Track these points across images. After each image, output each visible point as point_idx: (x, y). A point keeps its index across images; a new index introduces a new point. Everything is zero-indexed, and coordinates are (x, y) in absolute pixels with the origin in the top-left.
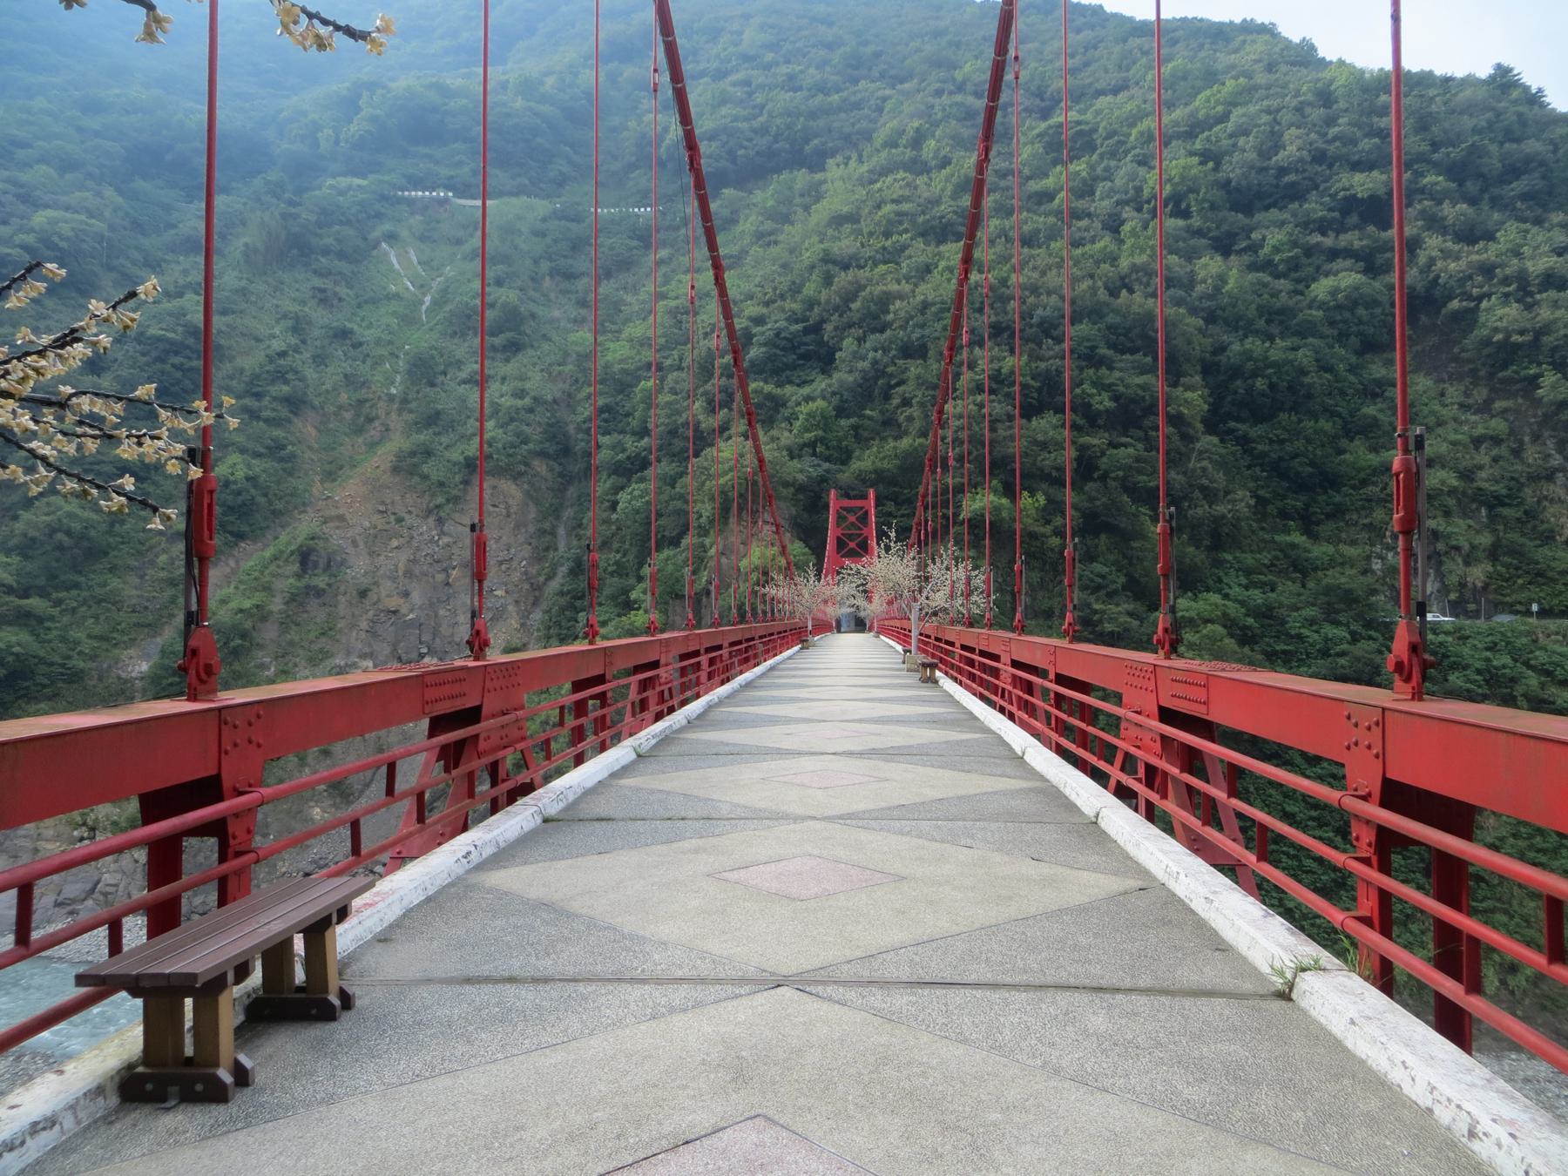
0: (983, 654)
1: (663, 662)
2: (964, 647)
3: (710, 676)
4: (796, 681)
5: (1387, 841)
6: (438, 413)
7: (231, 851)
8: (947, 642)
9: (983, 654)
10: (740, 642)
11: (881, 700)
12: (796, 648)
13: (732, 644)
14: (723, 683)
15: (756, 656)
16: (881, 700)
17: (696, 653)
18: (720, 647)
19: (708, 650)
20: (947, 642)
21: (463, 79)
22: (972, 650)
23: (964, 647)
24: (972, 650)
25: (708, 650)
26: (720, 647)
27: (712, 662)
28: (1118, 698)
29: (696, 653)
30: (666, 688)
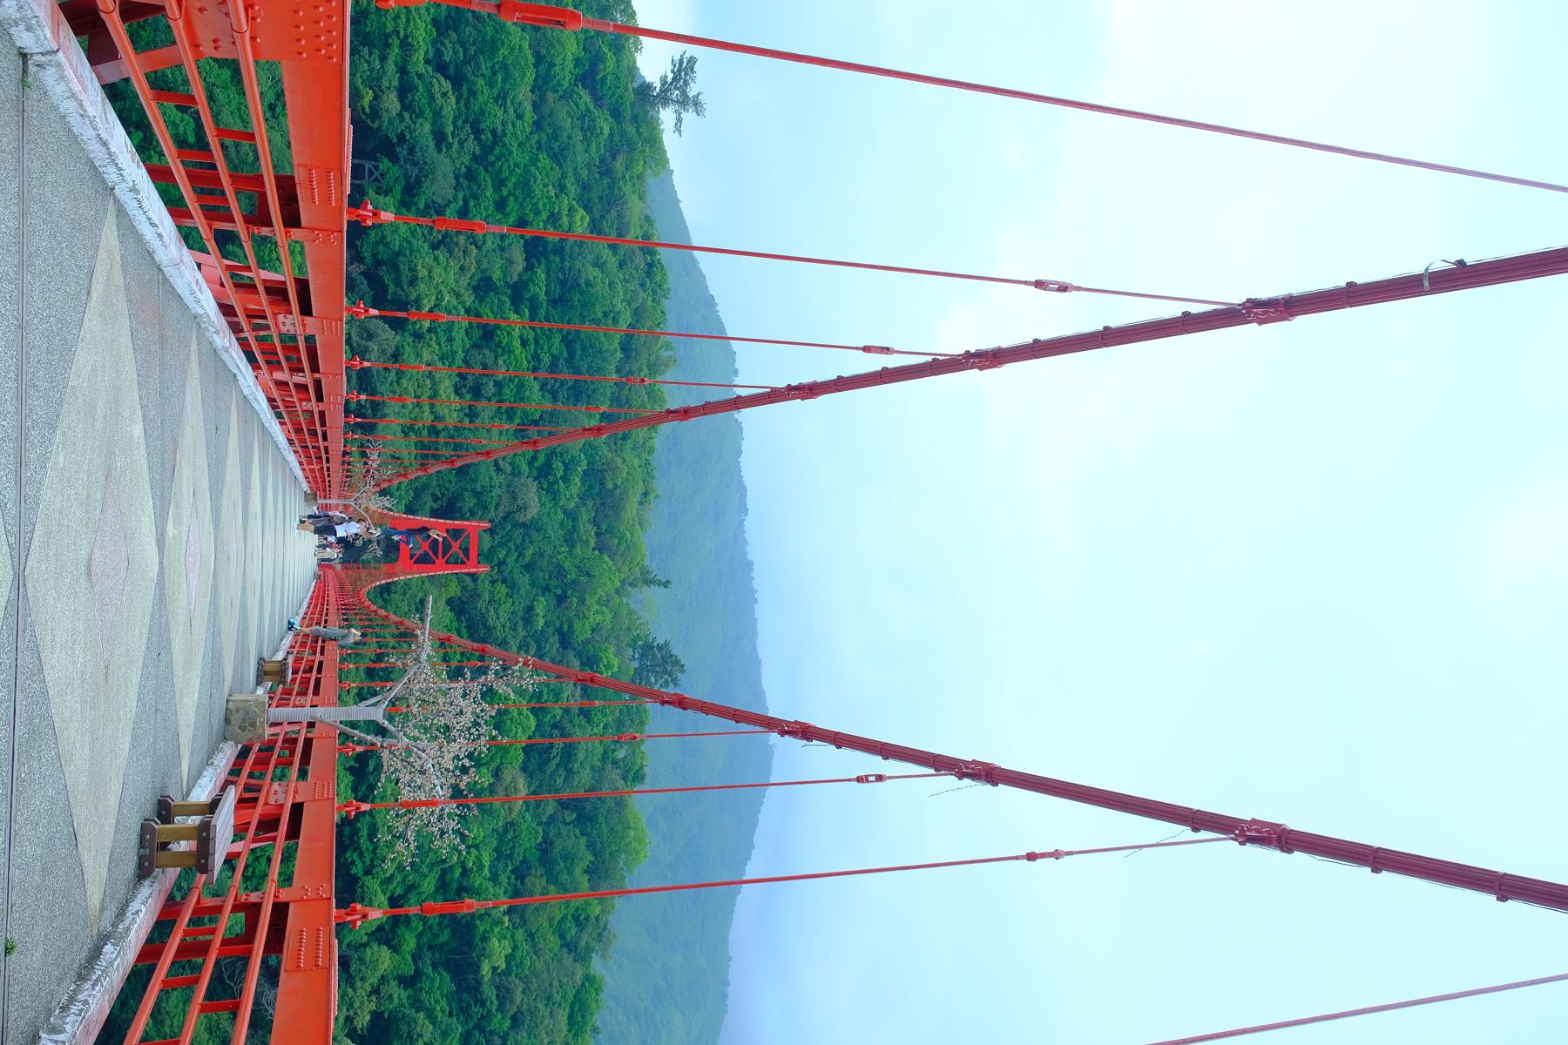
0: (318, 681)
1: (308, 319)
2: (321, 663)
3: (281, 385)
4: (270, 493)
5: (252, 910)
6: (578, 400)
7: (228, 141)
8: (323, 648)
9: (318, 681)
10: (323, 424)
11: (261, 615)
12: (305, 486)
13: (322, 414)
14: (271, 400)
15: (225, 241)
16: (261, 615)
17: (315, 368)
18: (320, 398)
19: (318, 384)
20: (323, 648)
21: (671, 325)
22: (319, 671)
23: (321, 663)
24: (319, 671)
25: (318, 384)
26: (320, 398)
27: (301, 388)
28: (303, 774)
29: (315, 368)
30: (270, 321)
